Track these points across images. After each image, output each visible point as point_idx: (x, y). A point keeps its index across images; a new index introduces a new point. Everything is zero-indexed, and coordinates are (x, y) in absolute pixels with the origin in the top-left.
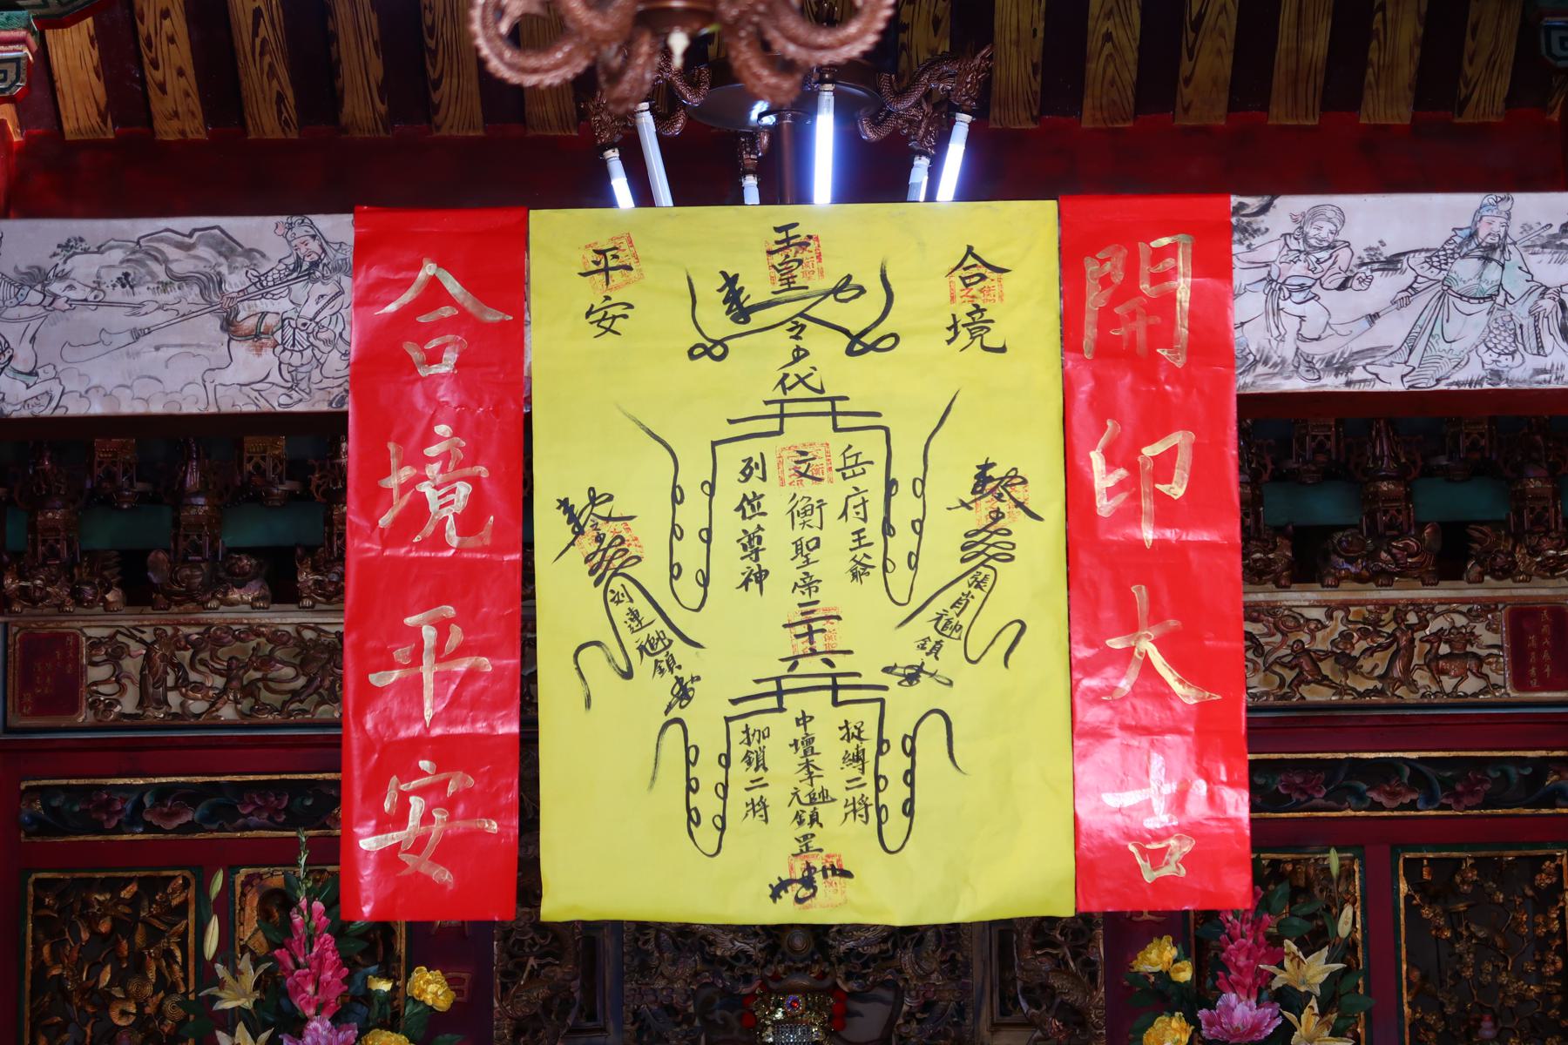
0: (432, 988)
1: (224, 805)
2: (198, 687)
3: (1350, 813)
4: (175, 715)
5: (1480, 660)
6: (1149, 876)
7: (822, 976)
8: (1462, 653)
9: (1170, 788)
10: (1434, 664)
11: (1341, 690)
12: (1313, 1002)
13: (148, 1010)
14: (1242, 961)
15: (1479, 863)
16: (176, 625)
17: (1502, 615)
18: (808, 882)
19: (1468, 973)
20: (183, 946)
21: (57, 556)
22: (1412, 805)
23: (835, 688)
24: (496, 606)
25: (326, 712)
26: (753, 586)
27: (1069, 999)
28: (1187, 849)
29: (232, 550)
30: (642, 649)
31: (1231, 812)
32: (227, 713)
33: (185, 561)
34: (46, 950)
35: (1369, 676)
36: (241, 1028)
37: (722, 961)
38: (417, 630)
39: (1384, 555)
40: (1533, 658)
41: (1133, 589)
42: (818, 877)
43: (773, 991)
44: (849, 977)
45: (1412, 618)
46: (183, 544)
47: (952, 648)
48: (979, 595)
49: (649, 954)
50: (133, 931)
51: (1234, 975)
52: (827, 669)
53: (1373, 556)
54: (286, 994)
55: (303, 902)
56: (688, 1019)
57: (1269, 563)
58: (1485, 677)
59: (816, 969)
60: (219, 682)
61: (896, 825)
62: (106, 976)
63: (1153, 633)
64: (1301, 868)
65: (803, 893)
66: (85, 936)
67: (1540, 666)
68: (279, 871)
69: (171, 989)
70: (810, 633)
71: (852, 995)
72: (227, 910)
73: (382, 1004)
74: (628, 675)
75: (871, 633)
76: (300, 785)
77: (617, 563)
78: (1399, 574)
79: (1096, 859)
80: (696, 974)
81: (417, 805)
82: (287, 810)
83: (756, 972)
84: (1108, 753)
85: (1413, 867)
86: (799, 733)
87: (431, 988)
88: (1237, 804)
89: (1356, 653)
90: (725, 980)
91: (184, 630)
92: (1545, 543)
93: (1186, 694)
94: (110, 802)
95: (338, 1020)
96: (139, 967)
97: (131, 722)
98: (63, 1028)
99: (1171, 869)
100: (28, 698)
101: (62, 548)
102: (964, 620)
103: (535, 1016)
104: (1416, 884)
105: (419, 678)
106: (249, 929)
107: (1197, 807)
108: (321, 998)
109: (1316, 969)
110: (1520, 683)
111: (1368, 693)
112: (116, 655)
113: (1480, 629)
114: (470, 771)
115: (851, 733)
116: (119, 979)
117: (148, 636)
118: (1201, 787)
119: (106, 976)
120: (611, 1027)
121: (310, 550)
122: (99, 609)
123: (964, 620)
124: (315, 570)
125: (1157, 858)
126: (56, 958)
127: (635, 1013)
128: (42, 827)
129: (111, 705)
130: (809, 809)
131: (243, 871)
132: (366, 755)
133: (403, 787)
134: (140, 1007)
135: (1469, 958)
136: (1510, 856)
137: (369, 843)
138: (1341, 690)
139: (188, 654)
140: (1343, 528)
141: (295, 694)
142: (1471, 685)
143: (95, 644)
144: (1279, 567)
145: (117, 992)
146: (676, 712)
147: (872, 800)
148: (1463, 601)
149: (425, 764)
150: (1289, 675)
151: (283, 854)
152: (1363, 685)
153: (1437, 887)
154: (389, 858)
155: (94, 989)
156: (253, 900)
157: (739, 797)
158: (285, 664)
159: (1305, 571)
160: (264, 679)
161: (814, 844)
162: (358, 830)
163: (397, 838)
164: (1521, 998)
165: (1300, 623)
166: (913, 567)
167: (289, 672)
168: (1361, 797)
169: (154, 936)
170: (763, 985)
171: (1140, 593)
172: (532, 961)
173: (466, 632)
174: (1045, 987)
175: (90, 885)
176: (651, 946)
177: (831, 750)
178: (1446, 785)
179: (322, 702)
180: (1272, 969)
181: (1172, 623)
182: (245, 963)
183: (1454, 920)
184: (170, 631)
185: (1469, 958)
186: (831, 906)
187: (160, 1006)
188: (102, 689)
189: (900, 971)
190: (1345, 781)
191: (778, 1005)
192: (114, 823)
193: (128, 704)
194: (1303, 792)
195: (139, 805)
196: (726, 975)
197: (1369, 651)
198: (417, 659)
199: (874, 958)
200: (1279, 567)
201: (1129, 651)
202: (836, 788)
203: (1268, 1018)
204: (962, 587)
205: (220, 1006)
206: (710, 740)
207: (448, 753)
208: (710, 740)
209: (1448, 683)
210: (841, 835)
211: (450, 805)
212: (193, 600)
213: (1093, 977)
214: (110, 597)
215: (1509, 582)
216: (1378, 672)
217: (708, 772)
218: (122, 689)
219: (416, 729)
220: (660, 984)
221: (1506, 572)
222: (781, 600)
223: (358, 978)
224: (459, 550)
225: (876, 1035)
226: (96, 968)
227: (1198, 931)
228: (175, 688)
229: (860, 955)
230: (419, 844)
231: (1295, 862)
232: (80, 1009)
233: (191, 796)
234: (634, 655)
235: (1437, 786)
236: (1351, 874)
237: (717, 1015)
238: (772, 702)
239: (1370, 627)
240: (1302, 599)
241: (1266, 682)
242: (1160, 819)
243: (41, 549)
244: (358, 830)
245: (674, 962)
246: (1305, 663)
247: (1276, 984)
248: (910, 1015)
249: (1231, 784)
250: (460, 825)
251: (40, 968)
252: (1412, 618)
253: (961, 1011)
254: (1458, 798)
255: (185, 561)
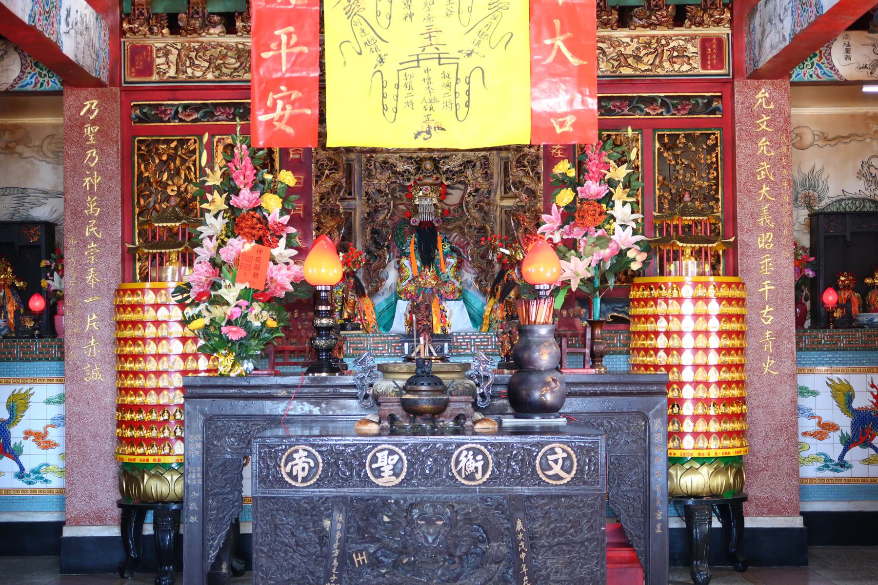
0: (288, 178)
1: (209, 112)
2: (198, 66)
3: (637, 116)
4: (190, 77)
5: (689, 58)
6: (559, 131)
7: (437, 179)
8: (682, 55)
9: (568, 97)
10: (671, 59)
11: (635, 69)
12: (621, 184)
13: (182, 189)
14: (594, 169)
15: (686, 136)
16: (190, 42)
17: (698, 41)
18: (428, 132)
19: (681, 177)
20: (194, 165)
21: (143, 14)
22: (661, 114)
23: (439, 58)
24: (310, 25)
25: (247, 76)
26: (408, 18)
27: (530, 186)
28: (573, 121)
29: (210, 13)
30: (365, 43)
31: (590, 107)
32: (210, 76)
33: (193, 17)
34: (142, 166)
35: (646, 64)
36: (216, 192)
37: (399, 173)
38: (279, 36)
39: (653, 17)
40: (709, 57)
41: (555, 21)
42: (432, 130)
43: (418, 185)
44: (447, 179)
45: (663, 42)
46: (191, 11)
47: (485, 42)
48: (495, 22)
49: (372, 170)
50: (175, 159)
51: (591, 174)
52: (437, 51)
53: (649, 17)
54: (232, 180)
55: (239, 145)
56: (386, 195)
57: (609, 20)
58: (691, 64)
59: (435, 176)
60: (207, 64)
61: (462, 110)
62: (165, 177)
63: (562, 38)
64: (619, 138)
65: (427, 136)
66: (157, 161)
67: (712, 60)
68: (230, 137)
69: (190, 182)
70: (430, 37)
71: (448, 186)
72: (209, 147)
73: (269, 184)
74: (360, 54)
75: (454, 39)
76: (233, 104)
77: (356, 10)
78: (659, 25)
79: (540, 123)
80: (389, 178)
81: (280, 103)
82: (233, 114)
83: (412, 177)
84: (544, 85)
85: (661, 137)
86: (425, 76)
87: (287, 178)
88: (593, 104)
89: (641, 55)
90: (400, 180)
91: (193, 44)
92: (715, 13)
93: (574, 61)
94: (165, 110)
95: (252, 189)
96: (178, 173)
97: (173, 80)
98: (149, 196)
99: (568, 128)
100: (133, 70)
101: (145, 11)
102: (489, 32)
103: (329, 193)
104: (663, 144)
105: (280, 55)
106: (219, 159)
107: (578, 106)
108: (246, 181)
109: (621, 173)
110: (704, 67)
111: (646, 70)
112: (166, 55)
113: (689, 46)
114: (300, 90)
115: (446, 76)
116: (171, 177)
117: (179, 47)
118: (579, 97)
119: (165, 177)
120: (357, 197)
121: (241, 14)
122: (160, 36)
123: (489, 32)
124: (243, 21)
125: (562, 125)
126: (146, 170)
127: (367, 193)
128: (141, 120)
129: (165, 73)
130: (429, 105)
131: (217, 137)
132: (260, 85)
133: (275, 97)
134: (179, 188)
135: (681, 172)
136: (698, 133)
137: (262, 118)
138: (635, 69)
139: (194, 54)
140: (638, 7)
141: (235, 69)
142: (685, 67)
143: (158, 50)
144: (613, 22)
145: (170, 182)
146: (378, 68)
147: (453, 101)
148: (684, 35)
149: (283, 88)
150: (616, 64)
151: (231, 131)
152: (644, 67)
153: (670, 145)
154: (269, 124)
155: (161, 182)
156: (221, 148)
157: (402, 100)
158: (232, 57)
159: (623, 23)
160: (224, 63)
161: (431, 118)
162: (258, 113)
163: (275, 116)
164: (700, 187)
165: (620, 43)
166: (470, 12)
167: (233, 61)
168: (642, 110)
169: (184, 161)
170: (415, 182)
171: (557, 22)
172: (327, 172)
173: (298, 37)
174: (520, 182)
175: (158, 141)
176: (372, 167)
177: (438, 82)
178: (675, 106)
179: (246, 72)
180: (606, 172)
181: (569, 34)
182: (217, 168)
183: (676, 157)
184: (187, 45)
185: (681, 172)
186: (437, 142)
187: (186, 188)
188: (161, 67)
189: (466, 177)
190: (635, 104)
191: (420, 190)
192: (167, 118)
193: (172, 73)
194: (620, 108)
195: (177, 112)
196: (401, 178)
197: (647, 54)
198: (279, 46)
199: (457, 172)
200: (613, 22)
201: (553, 45)
202: (440, 97)
203: (603, 190)
204: (489, 19)
205: (207, 184)
206: (391, 80)
207: (292, 84)
208: (391, 80)
209: (676, 67)
210: (442, 115)
211: (292, 103)
212: (196, 32)
213: (539, 179)
214: (164, 31)
215: (701, 28)
216: (650, 62)
217: (390, 90)
218: (169, 67)
219: (279, 75)
220: (376, 181)
221: (701, 24)
222: (419, 24)
223: (260, 174)
224: (295, 5)
225: (457, 202)
226: (162, 173)
227: (577, 155)
228: (190, 66)
229: (451, 171)
230: (281, 119)
231: (616, 135)
232: (156, 189)
233: (197, 108)
234: (362, 46)
235: (671, 106)
236: (637, 140)
237: (397, 194)
238: (415, 64)
239: (647, 45)
240: (621, 34)
241: (607, 66)
242: (564, 108)
243: (137, 12)
244: (258, 113)
245: (381, 174)
246: (621, 59)
247: (607, 178)
248: (470, 193)
249: (591, 96)
250: (297, 111)
251: (140, 174)
252: (663, 42)
253: (489, 192)
254: (679, 110)
255: (193, 17)
